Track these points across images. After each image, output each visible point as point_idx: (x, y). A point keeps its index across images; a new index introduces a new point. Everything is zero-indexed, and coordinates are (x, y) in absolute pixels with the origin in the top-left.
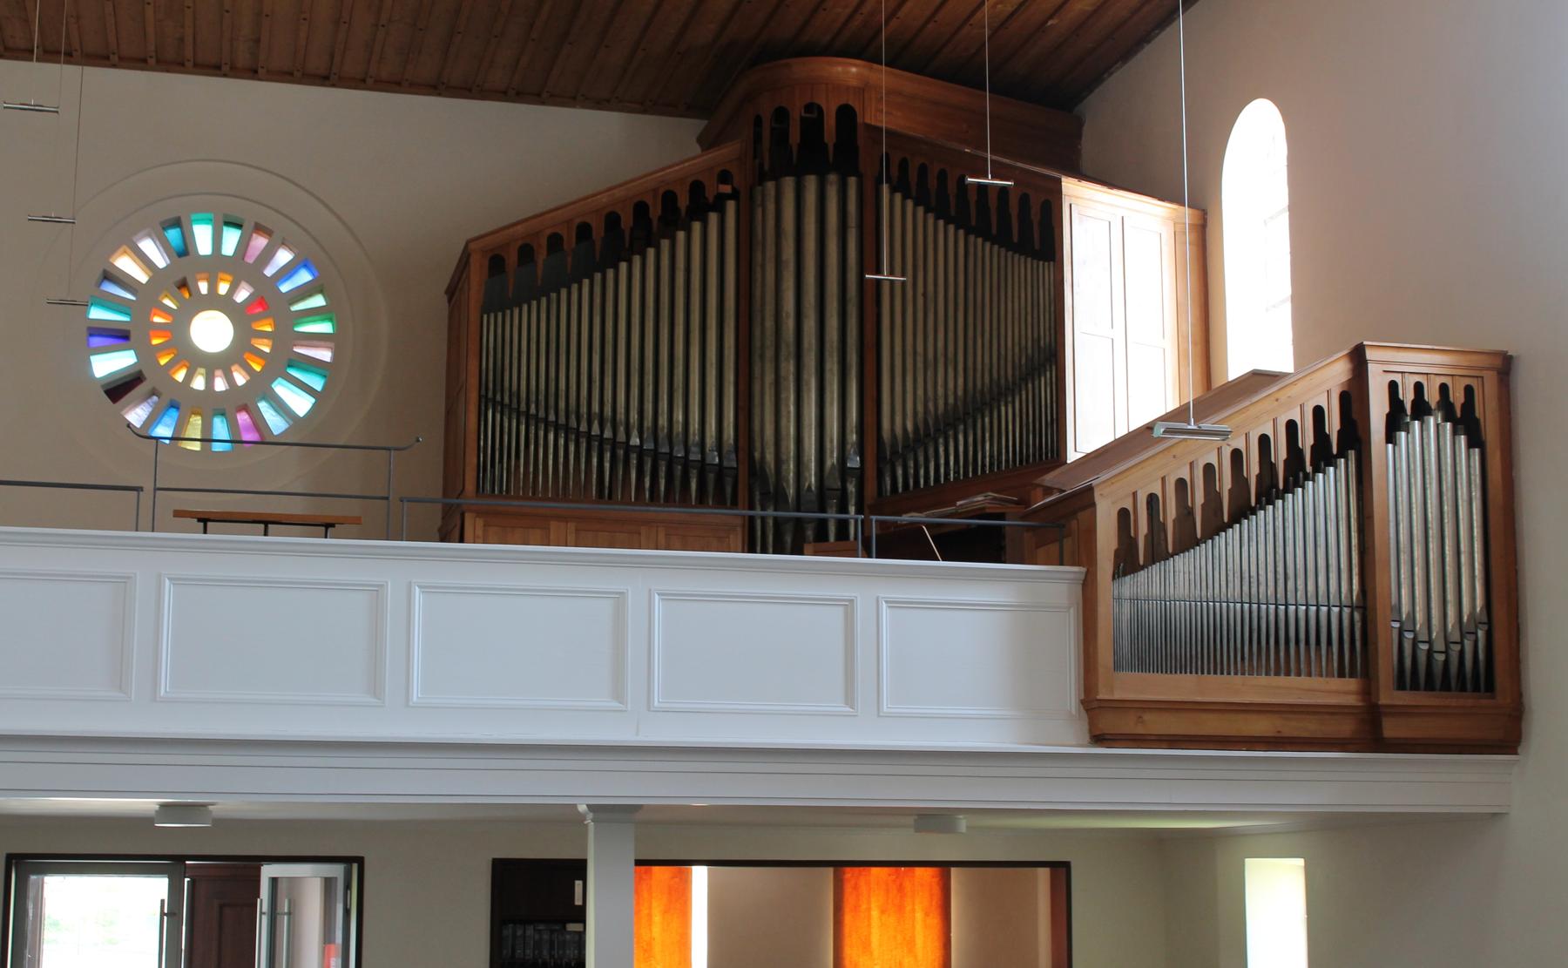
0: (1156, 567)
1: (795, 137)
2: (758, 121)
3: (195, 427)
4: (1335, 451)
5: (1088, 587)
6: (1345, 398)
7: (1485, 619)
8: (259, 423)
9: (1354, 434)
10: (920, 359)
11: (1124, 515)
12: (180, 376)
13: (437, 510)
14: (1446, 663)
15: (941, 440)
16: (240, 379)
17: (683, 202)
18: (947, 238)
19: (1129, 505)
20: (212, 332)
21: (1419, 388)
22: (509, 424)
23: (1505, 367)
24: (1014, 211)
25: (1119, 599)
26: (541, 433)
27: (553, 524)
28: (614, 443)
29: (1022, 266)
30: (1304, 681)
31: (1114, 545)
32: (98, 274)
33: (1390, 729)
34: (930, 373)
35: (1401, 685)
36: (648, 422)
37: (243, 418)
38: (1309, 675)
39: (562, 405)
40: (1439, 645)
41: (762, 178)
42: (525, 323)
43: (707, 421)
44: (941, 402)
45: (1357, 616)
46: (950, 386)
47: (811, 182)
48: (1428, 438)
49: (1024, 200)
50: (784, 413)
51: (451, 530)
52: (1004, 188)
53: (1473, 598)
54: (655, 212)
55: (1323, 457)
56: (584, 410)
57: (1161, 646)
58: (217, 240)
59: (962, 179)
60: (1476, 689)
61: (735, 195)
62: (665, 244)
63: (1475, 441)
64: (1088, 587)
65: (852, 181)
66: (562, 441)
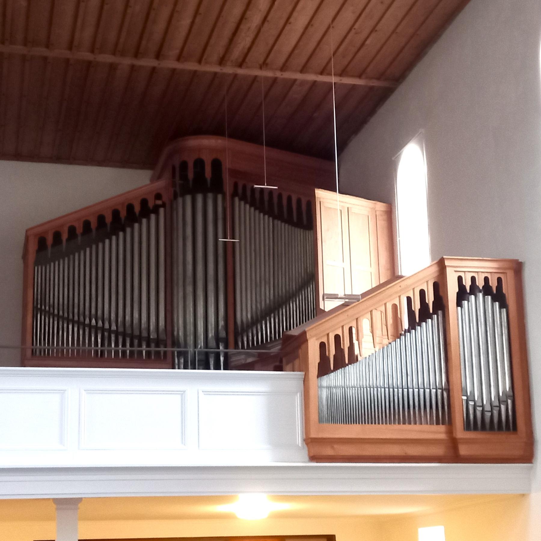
0: (339, 371)
1: (191, 175)
2: (174, 168)
4: (431, 311)
5: (306, 381)
7: (511, 394)
9: (440, 303)
10: (254, 283)
11: (322, 346)
15: (263, 322)
17: (137, 209)
18: (265, 221)
19: (325, 340)
21: (473, 279)
23: (517, 268)
24: (275, 200)
25: (321, 387)
26: (65, 325)
28: (103, 329)
29: (299, 233)
30: (418, 427)
31: (318, 360)
33: (463, 450)
34: (258, 289)
36: (120, 319)
38: (415, 423)
39: (76, 310)
40: (488, 408)
41: (175, 197)
42: (57, 270)
44: (263, 303)
45: (445, 394)
46: (267, 295)
47: (200, 198)
48: (477, 303)
49: (280, 196)
50: (188, 312)
52: (271, 191)
53: (505, 384)
55: (425, 314)
56: (87, 313)
57: (347, 412)
59: (253, 186)
61: (164, 205)
62: (128, 230)
63: (504, 305)
64: (306, 381)
65: (220, 197)
66: (76, 329)
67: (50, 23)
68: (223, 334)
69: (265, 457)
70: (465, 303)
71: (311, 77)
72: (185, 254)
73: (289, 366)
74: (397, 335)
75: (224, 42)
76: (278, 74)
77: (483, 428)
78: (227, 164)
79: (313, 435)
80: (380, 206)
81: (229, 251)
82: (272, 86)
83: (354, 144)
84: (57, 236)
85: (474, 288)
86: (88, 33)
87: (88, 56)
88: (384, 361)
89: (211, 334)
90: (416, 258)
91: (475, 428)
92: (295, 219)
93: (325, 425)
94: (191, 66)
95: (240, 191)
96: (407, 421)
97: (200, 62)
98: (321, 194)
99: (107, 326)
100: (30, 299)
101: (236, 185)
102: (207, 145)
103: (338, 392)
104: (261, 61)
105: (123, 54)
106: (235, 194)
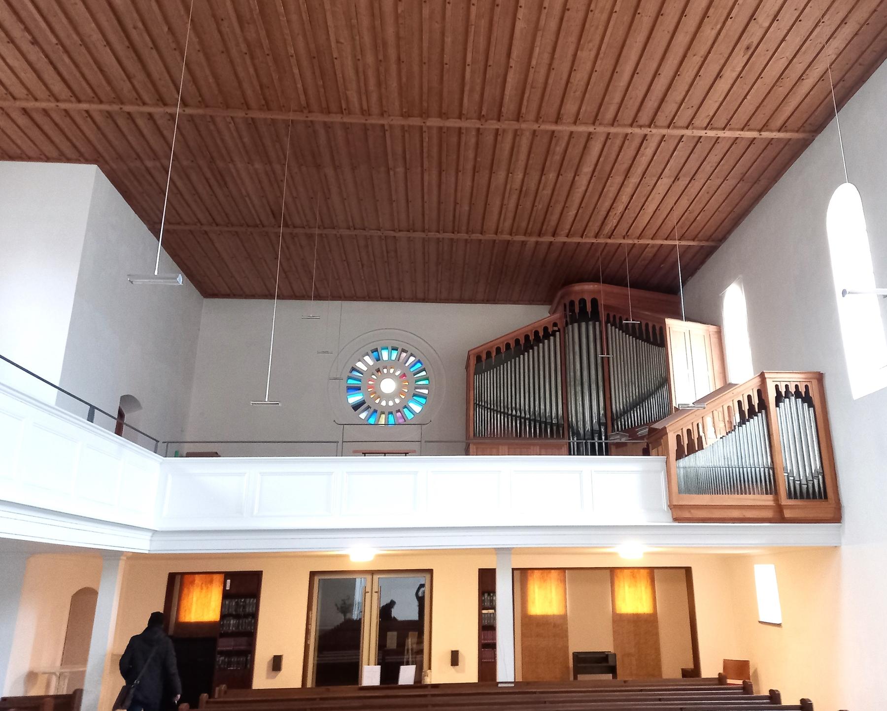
0: (692, 456)
1: (577, 310)
2: (565, 305)
6: (759, 392)
9: (763, 405)
13: (464, 444)
14: (807, 488)
16: (397, 401)
17: (541, 334)
18: (630, 340)
20: (388, 386)
21: (787, 386)
22: (495, 414)
23: (820, 378)
25: (679, 467)
27: (500, 447)
28: (520, 417)
29: (655, 349)
33: (787, 514)
35: (790, 496)
40: (804, 482)
41: (567, 325)
42: (489, 377)
43: (551, 408)
45: (771, 472)
46: (634, 392)
47: (583, 325)
51: (467, 453)
53: (816, 464)
54: (532, 338)
55: (752, 413)
58: (390, 355)
60: (821, 498)
61: (559, 330)
62: (536, 348)
63: (811, 405)
64: (667, 462)
65: (597, 323)
67: (484, 218)
68: (603, 420)
69: (643, 520)
70: (781, 404)
71: (659, 242)
73: (654, 451)
75: (599, 223)
76: (636, 241)
78: (602, 302)
79: (675, 503)
80: (712, 328)
81: (605, 363)
82: (632, 248)
83: (691, 282)
85: (788, 394)
86: (508, 224)
87: (508, 237)
88: (725, 449)
91: (796, 497)
95: (612, 319)
96: (743, 492)
99: (523, 415)
100: (472, 398)
101: (608, 315)
102: (588, 289)
103: (692, 474)
105: (530, 235)
106: (608, 321)
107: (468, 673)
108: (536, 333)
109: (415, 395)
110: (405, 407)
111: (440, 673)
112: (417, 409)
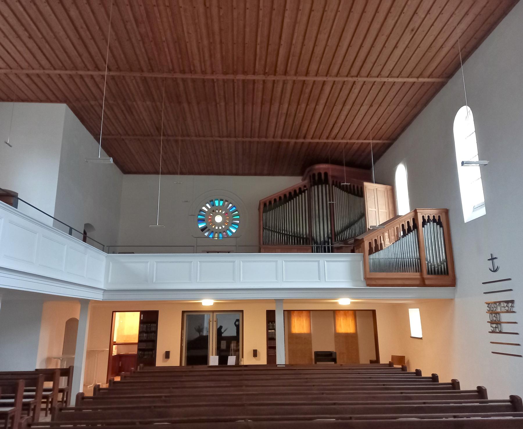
1: (317, 178)
3: (216, 235)
6: (414, 220)
8: (227, 234)
9: (416, 226)
11: (370, 243)
12: (217, 228)
17: (298, 191)
21: (428, 216)
23: (447, 212)
25: (370, 259)
29: (358, 198)
30: (408, 273)
32: (199, 210)
33: (427, 282)
35: (428, 273)
37: (224, 233)
40: (436, 266)
41: (311, 186)
42: (271, 215)
43: (303, 229)
46: (346, 222)
47: (320, 186)
48: (430, 226)
53: (443, 256)
55: (409, 230)
58: (219, 203)
60: (445, 274)
61: (307, 190)
62: (295, 199)
63: (441, 226)
64: (364, 256)
65: (327, 186)
68: (330, 236)
71: (361, 141)
72: (315, 206)
73: (357, 251)
74: (398, 239)
75: (328, 131)
76: (349, 141)
77: (438, 273)
78: (330, 173)
80: (389, 187)
81: (332, 206)
83: (376, 164)
84: (270, 202)
89: (326, 236)
90: (404, 208)
91: (432, 274)
92: (356, 192)
93: (372, 273)
94: (317, 140)
95: (335, 183)
97: (319, 139)
98: (366, 184)
101: (333, 182)
102: (322, 167)
104: (342, 136)
105: (292, 138)
106: (333, 184)
107: (262, 360)
108: (295, 191)
109: (232, 224)
110: (228, 230)
111: (247, 360)
112: (234, 231)
